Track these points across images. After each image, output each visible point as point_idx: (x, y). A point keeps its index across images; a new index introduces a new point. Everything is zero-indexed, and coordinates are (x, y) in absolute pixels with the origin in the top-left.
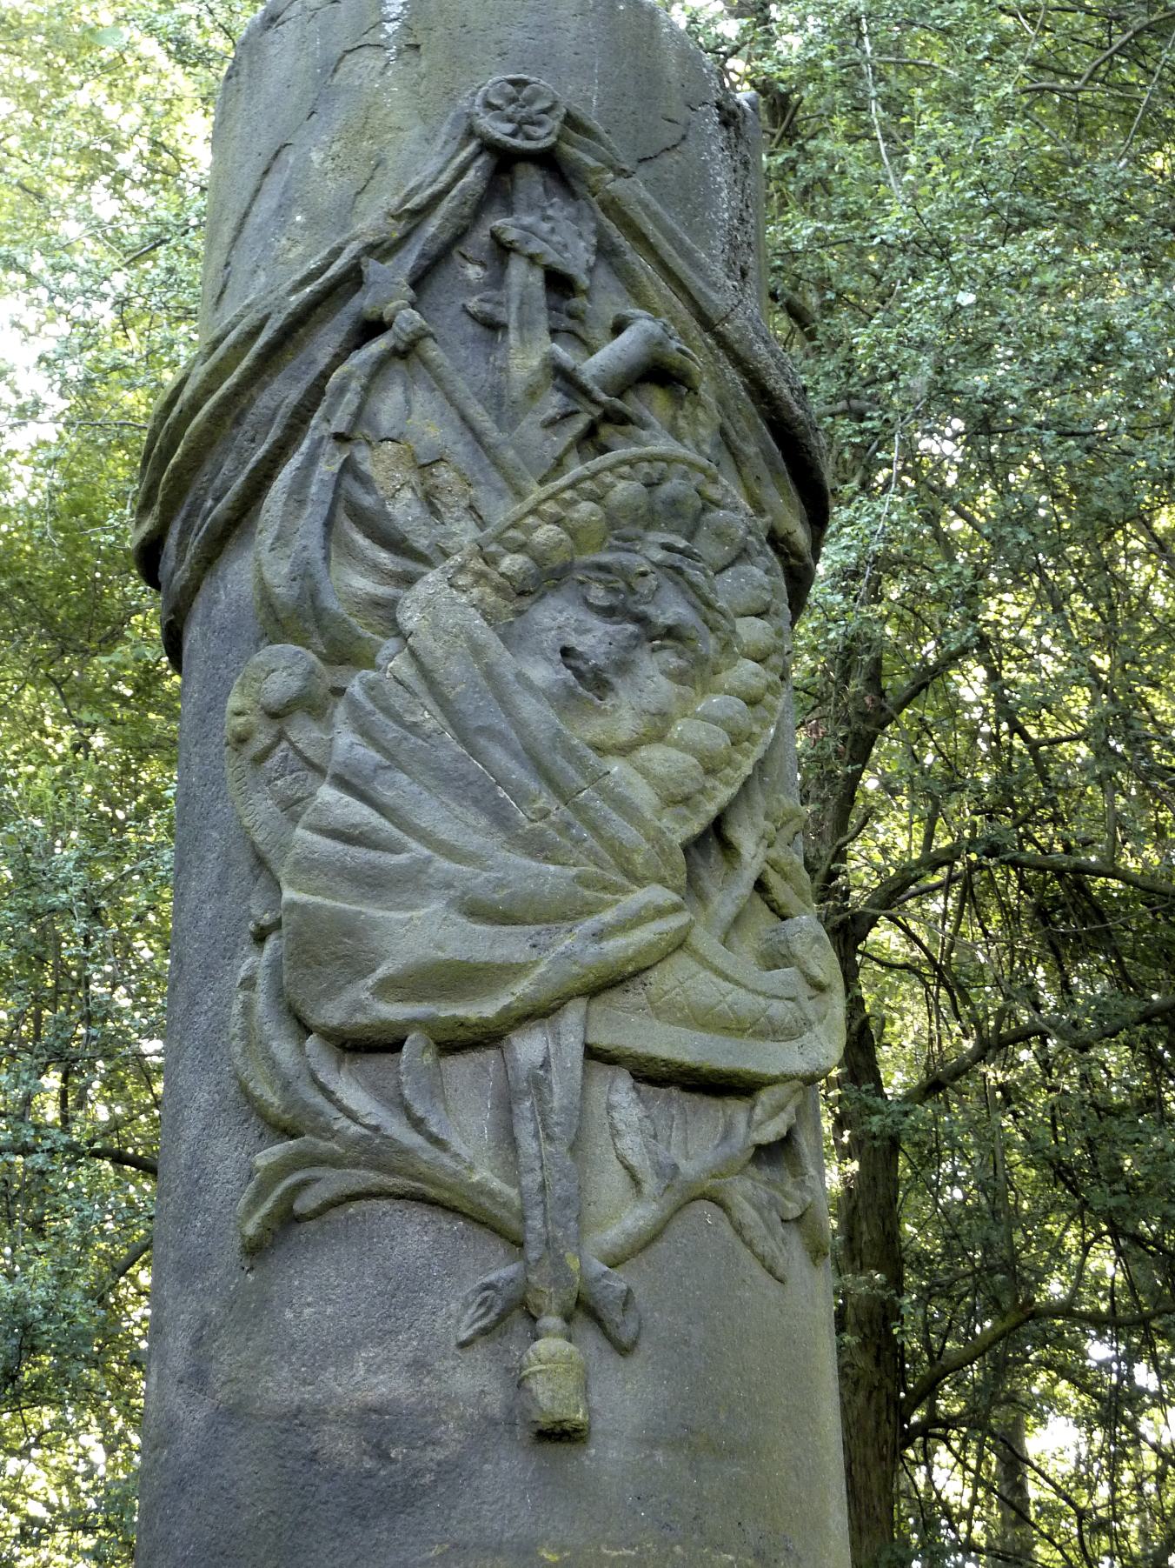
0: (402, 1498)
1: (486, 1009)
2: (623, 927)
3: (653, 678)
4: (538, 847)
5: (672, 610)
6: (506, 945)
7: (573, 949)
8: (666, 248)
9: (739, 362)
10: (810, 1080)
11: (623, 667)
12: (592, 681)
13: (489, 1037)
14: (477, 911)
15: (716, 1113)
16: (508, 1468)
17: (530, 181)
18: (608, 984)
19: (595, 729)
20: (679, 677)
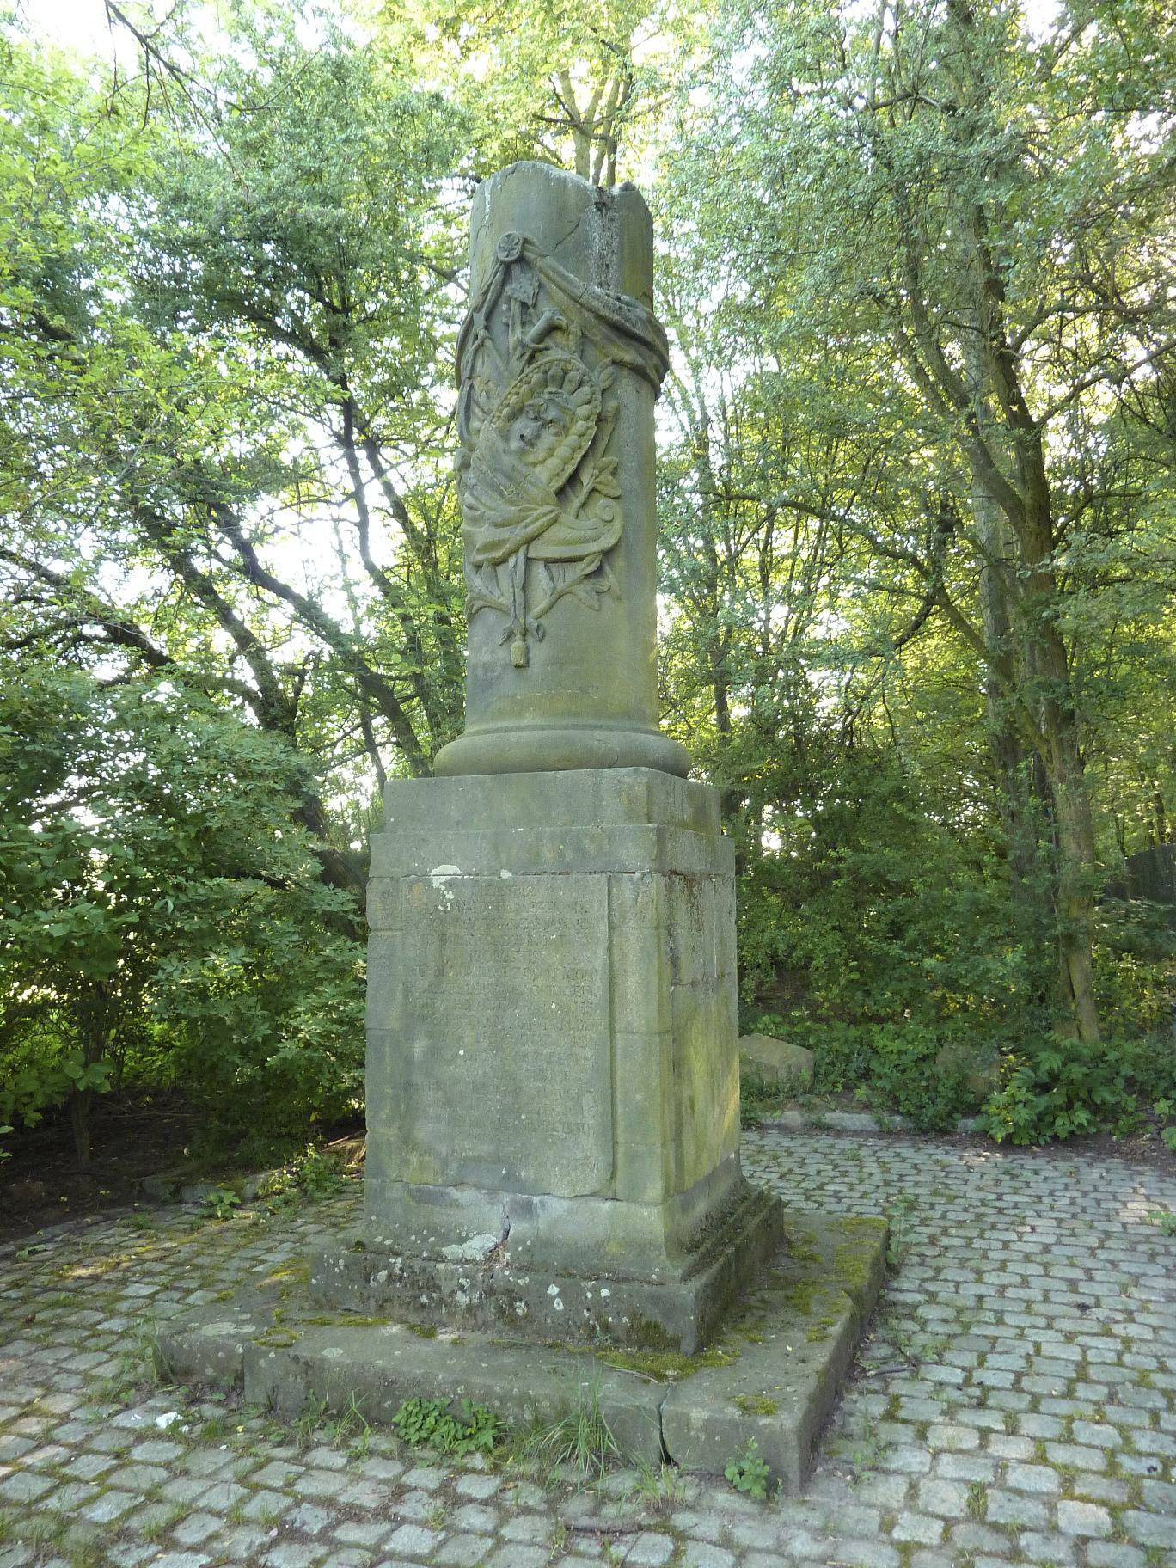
0: (490, 685)
1: (498, 554)
2: (532, 522)
3: (548, 437)
4: (512, 502)
5: (552, 413)
6: (503, 533)
7: (521, 532)
8: (558, 279)
9: (589, 310)
10: (471, 617)
11: (538, 437)
12: (529, 442)
13: (504, 560)
14: (497, 525)
15: (570, 568)
16: (511, 675)
17: (516, 270)
18: (530, 541)
19: (531, 459)
20: (557, 434)
